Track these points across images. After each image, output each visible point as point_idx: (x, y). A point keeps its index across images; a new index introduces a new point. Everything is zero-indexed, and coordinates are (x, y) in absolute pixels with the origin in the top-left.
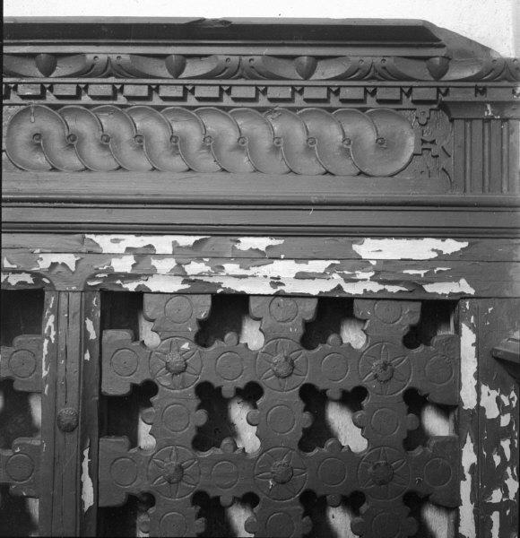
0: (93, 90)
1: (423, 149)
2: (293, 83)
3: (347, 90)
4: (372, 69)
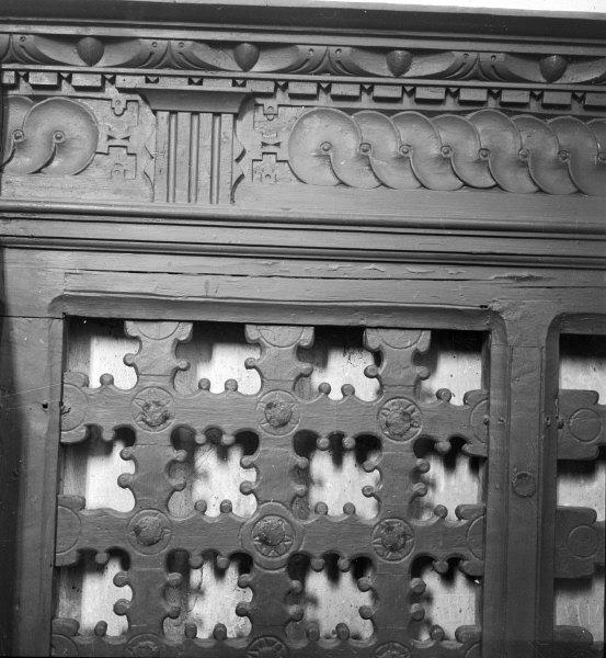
0: (33, 79)
1: (264, 153)
2: (232, 75)
3: (552, 94)
4: (327, 58)
